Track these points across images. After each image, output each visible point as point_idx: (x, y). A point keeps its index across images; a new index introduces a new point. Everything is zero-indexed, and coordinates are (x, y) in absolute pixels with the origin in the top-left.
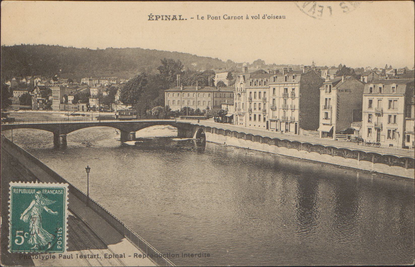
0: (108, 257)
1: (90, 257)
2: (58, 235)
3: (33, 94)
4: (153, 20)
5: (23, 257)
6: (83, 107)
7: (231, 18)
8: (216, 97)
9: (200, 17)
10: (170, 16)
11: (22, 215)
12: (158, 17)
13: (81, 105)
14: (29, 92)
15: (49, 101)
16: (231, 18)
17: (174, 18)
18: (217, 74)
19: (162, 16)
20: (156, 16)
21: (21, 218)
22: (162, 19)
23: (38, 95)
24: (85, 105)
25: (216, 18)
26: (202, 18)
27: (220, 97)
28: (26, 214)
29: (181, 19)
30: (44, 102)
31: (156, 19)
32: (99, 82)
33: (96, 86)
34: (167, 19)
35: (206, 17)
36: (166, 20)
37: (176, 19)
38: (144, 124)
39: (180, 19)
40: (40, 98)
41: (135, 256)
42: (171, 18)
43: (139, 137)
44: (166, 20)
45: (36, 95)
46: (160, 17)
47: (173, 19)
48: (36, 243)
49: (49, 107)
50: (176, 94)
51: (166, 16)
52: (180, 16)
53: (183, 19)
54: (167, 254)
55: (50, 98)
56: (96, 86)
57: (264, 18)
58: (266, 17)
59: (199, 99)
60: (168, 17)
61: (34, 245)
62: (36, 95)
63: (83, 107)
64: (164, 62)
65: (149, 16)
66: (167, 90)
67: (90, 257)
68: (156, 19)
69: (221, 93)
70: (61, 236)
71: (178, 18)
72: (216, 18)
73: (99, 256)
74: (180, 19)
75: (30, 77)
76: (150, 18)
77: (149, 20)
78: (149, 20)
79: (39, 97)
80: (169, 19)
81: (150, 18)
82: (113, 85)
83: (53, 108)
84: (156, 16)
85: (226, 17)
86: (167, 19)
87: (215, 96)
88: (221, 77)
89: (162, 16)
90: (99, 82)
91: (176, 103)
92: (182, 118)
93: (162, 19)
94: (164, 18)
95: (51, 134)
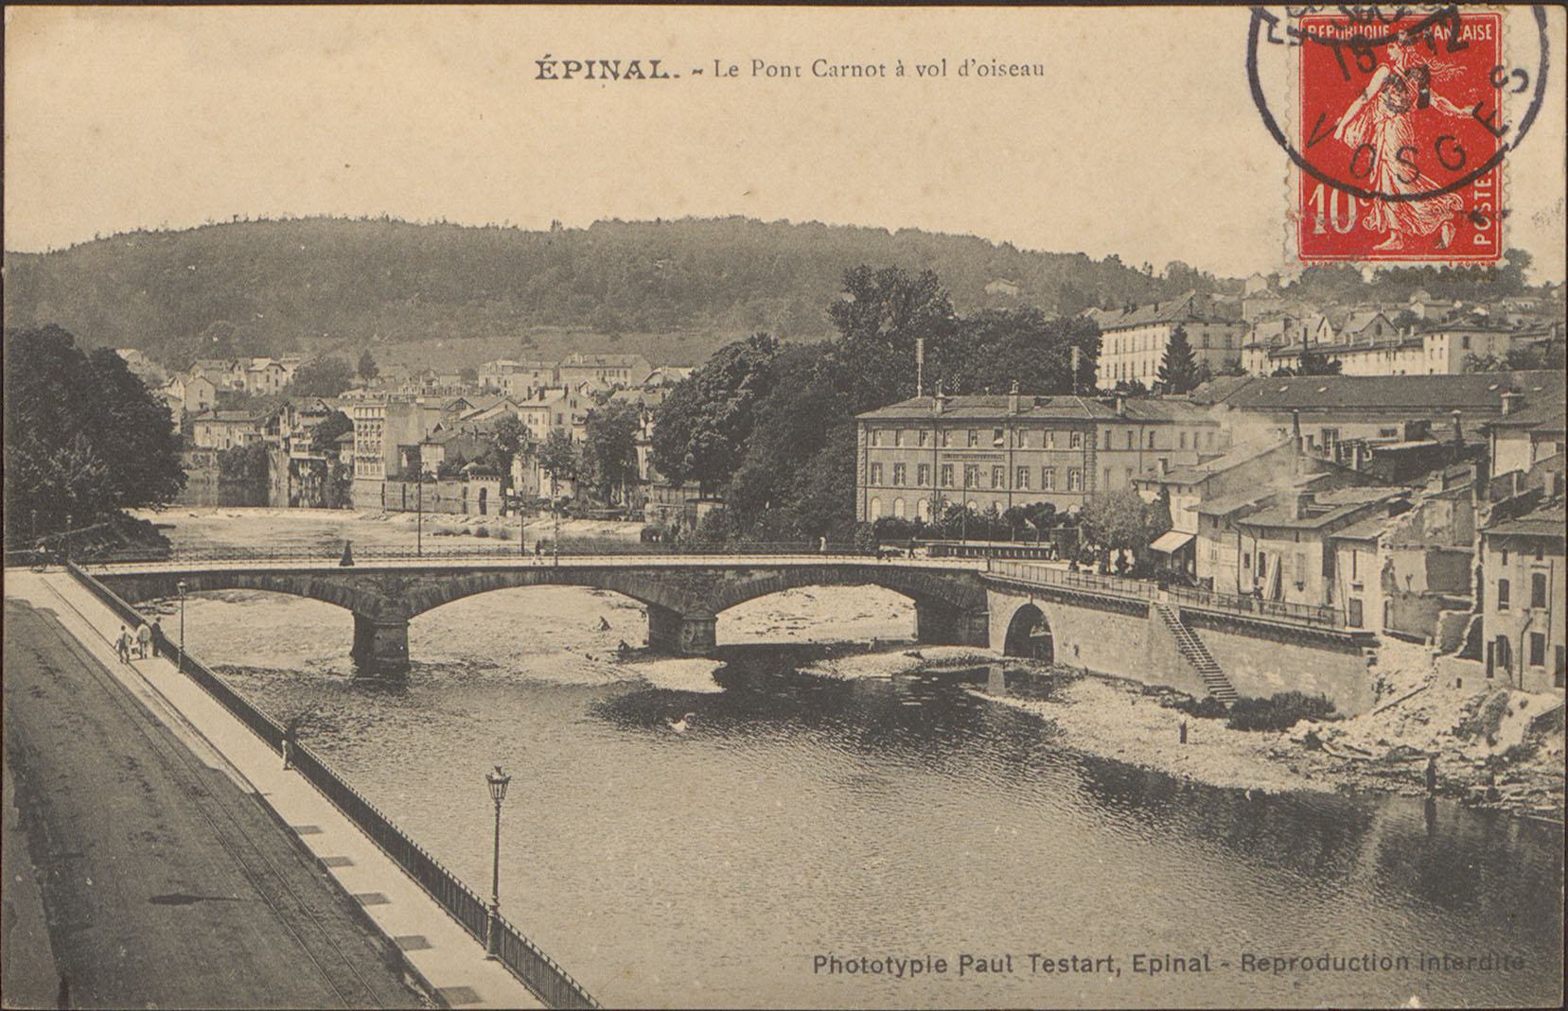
0: (1146, 965)
1: (1079, 965)
2: (1477, 195)
3: (273, 438)
4: (555, 77)
5: (827, 967)
6: (484, 491)
7: (840, 71)
8: (1108, 449)
9: (724, 69)
10: (617, 63)
11: (1342, 122)
12: (573, 66)
13: (475, 486)
14: (257, 428)
15: (340, 469)
16: (840, 71)
17: (635, 70)
18: (1108, 339)
19: (590, 64)
20: (567, 64)
21: (1338, 135)
22: (590, 76)
23: (294, 441)
24: (493, 487)
25: (785, 71)
26: (733, 71)
27: (1130, 449)
28: (1357, 118)
29: (660, 73)
30: (320, 469)
31: (567, 76)
32: (557, 378)
33: (542, 397)
34: (608, 73)
35: (746, 68)
36: (604, 76)
37: (641, 76)
38: (758, 575)
39: (654, 76)
40: (305, 455)
41: (1244, 962)
42: (623, 70)
43: (730, 641)
44: (604, 76)
45: (287, 440)
46: (579, 67)
47: (627, 77)
48: (1394, 225)
49: (338, 495)
50: (909, 437)
51: (605, 63)
52: (655, 63)
53: (666, 76)
54: (1365, 959)
55: (345, 456)
56: (542, 397)
57: (964, 70)
58: (973, 70)
59: (1021, 460)
60: (613, 66)
61: (1389, 230)
62: (287, 440)
63: (484, 491)
64: (857, 280)
65: (541, 64)
66: (892, 412)
67: (1079, 965)
68: (567, 76)
69: (1136, 428)
70: (1486, 200)
71: (646, 69)
72: (785, 71)
73: (1115, 965)
74: (654, 76)
75: (261, 363)
76: (544, 69)
77: (541, 77)
78: (541, 77)
79: (299, 448)
80: (616, 75)
81: (544, 69)
82: (617, 396)
83: (356, 501)
84: (567, 64)
85: (821, 68)
86: (608, 73)
87: (1101, 445)
88: (1133, 353)
89: (590, 64)
90: (557, 378)
91: (912, 474)
92: (936, 552)
93: (590, 76)
94: (597, 69)
95: (341, 620)
